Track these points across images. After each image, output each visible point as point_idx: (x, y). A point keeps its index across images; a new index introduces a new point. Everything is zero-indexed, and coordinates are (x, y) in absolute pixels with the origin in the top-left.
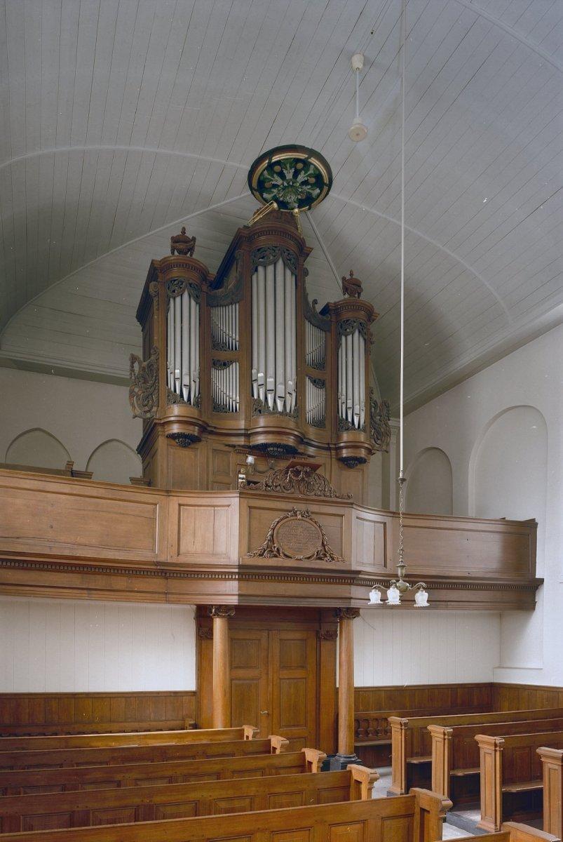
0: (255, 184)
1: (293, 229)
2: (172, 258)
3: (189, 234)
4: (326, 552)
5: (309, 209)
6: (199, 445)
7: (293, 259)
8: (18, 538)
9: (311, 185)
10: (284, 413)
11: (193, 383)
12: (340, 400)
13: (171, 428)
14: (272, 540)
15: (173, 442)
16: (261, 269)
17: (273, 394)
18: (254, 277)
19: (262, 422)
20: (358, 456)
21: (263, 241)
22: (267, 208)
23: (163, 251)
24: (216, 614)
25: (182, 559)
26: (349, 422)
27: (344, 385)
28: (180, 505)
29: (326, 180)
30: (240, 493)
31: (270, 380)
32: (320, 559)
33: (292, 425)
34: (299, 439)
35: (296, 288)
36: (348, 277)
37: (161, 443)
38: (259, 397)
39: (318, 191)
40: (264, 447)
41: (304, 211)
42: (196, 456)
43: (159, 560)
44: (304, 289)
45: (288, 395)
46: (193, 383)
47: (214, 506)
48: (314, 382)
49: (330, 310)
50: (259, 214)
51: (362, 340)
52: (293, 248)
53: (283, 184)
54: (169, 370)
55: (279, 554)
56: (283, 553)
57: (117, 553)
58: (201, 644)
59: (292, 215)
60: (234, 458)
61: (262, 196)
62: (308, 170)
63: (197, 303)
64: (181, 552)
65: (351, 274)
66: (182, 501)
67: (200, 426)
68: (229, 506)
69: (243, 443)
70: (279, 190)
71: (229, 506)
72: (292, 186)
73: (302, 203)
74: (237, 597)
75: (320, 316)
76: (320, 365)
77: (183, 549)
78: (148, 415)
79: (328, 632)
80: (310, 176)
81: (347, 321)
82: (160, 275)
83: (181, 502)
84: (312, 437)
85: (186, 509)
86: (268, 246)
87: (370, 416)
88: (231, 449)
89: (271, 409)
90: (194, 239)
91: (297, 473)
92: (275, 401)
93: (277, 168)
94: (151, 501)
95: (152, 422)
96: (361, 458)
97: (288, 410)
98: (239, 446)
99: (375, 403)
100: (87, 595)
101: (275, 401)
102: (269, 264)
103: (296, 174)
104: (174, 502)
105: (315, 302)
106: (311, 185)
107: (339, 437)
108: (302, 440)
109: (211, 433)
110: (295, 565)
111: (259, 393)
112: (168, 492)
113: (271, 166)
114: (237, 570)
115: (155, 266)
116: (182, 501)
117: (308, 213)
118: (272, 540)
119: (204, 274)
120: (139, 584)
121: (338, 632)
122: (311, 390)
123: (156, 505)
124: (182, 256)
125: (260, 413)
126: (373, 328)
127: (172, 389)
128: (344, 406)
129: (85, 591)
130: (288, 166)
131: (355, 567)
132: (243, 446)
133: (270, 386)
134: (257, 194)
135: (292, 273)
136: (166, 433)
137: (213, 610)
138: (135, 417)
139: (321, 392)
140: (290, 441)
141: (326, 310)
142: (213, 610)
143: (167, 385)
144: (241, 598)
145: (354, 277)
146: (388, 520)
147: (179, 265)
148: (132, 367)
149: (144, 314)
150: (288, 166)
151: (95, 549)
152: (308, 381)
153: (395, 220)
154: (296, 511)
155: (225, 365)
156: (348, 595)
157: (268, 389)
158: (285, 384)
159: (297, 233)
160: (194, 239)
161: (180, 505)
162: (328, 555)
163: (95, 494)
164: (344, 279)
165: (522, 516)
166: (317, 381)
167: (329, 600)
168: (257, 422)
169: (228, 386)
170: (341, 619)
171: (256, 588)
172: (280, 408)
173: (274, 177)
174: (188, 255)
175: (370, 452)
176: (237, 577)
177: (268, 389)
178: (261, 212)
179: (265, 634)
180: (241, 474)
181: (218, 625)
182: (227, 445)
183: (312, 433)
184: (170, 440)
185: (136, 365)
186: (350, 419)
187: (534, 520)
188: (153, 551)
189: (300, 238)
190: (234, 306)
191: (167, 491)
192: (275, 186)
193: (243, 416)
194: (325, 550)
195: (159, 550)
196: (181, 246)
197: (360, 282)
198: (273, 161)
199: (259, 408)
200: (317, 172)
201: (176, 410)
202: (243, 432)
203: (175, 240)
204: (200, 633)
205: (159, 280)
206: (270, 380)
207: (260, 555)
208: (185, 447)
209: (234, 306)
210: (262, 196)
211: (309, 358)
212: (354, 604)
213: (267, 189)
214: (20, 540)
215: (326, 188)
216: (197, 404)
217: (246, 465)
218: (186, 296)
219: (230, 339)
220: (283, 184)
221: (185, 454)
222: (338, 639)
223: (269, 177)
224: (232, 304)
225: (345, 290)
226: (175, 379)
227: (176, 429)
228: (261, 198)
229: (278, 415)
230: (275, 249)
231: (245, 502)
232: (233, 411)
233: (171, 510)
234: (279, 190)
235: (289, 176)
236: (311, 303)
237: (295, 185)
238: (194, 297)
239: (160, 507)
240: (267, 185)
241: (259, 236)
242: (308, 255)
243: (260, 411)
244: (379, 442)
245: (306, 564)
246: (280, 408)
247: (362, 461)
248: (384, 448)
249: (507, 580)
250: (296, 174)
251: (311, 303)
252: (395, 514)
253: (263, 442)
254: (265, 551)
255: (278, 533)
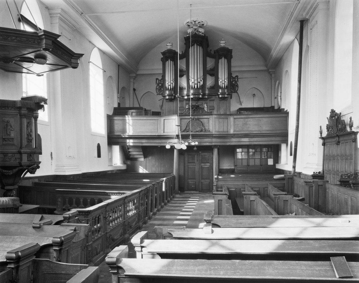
25: (165, 134)
64: (165, 132)
76: (212, 70)
104: (162, 119)
116: (164, 118)
148: (156, 81)
169: (183, 82)
172: (196, 87)
179: (38, 102)
218: (169, 60)
221: (171, 104)
245: (197, 133)
246: (196, 87)
249: (268, 131)
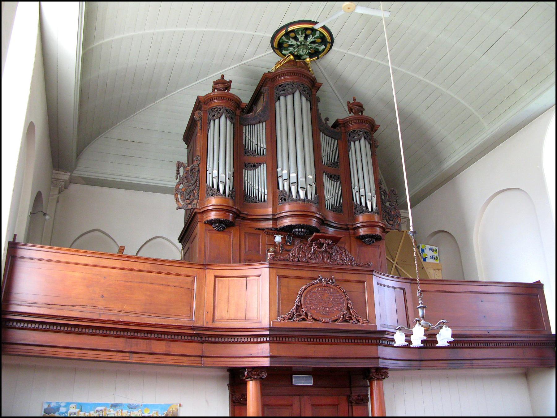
0: (276, 45)
1: (306, 71)
2: (214, 94)
3: (227, 78)
4: (351, 315)
5: (318, 59)
6: (233, 230)
7: (307, 90)
8: (73, 306)
9: (318, 43)
10: (306, 200)
11: (227, 180)
12: (353, 190)
13: (209, 215)
14: (300, 306)
15: (210, 227)
16: (282, 98)
17: (296, 186)
18: (277, 104)
19: (287, 208)
20: (374, 234)
21: (283, 79)
22: (285, 59)
23: (206, 90)
24: (250, 377)
26: (363, 207)
27: (355, 172)
28: (215, 277)
29: (329, 39)
30: (270, 264)
31: (293, 175)
32: (346, 321)
33: (314, 209)
34: (320, 221)
35: (311, 110)
36: (352, 101)
37: (199, 229)
38: (284, 188)
39: (323, 47)
40: (291, 227)
41: (315, 61)
42: (230, 237)
43: (195, 325)
44: (318, 110)
45: (309, 186)
46: (227, 180)
47: (246, 277)
48: (330, 177)
49: (339, 124)
50: (279, 64)
51: (367, 144)
52: (307, 84)
53: (297, 44)
54: (208, 172)
55: (307, 317)
56: (311, 316)
57: (157, 320)
58: (234, 409)
59: (305, 63)
60: (263, 239)
61: (281, 53)
62: (315, 35)
63: (231, 123)
64: (216, 318)
65: (354, 100)
66: (218, 273)
67: (234, 213)
68: (259, 276)
69: (271, 226)
70: (294, 48)
71: (259, 276)
72: (303, 45)
73: (311, 55)
74: (268, 359)
75: (332, 129)
76: (334, 165)
77: (217, 315)
78: (190, 207)
79: (359, 396)
80: (317, 38)
81: (354, 131)
82: (203, 106)
83: (217, 274)
84: (331, 220)
85: (221, 280)
86: (287, 83)
87: (381, 202)
88: (261, 231)
89: (294, 197)
90: (230, 81)
91: (320, 245)
92: (298, 192)
93: (292, 35)
94: (190, 274)
95: (194, 210)
96: (377, 235)
97: (309, 198)
98: (268, 229)
99: (384, 192)
100: (128, 358)
101: (298, 192)
102: (289, 94)
103: (306, 37)
104: (210, 275)
105: (327, 119)
106: (318, 43)
107: (355, 220)
108: (323, 222)
109: (243, 218)
110: (323, 327)
111: (284, 186)
112: (205, 266)
113: (287, 34)
114: (268, 333)
115: (200, 100)
116: (218, 273)
117: (317, 61)
118: (300, 306)
119: (237, 103)
120: (177, 348)
121: (369, 396)
122: (327, 182)
123: (194, 277)
124: (220, 92)
125: (285, 201)
126: (375, 135)
127: (211, 185)
128: (357, 194)
129: (128, 354)
130: (300, 33)
131: (379, 328)
132: (271, 229)
133: (293, 180)
134: (278, 51)
135: (307, 100)
136: (204, 220)
137: (246, 373)
138: (178, 209)
139: (338, 185)
140: (314, 223)
141: (336, 124)
142: (246, 373)
143: (206, 182)
144: (272, 360)
145: (356, 101)
146: (407, 286)
147: (218, 98)
149: (189, 137)
150: (300, 33)
151: (139, 315)
152: (325, 176)
153: (385, 63)
154: (321, 279)
155: (255, 167)
156: (375, 356)
157: (291, 182)
158: (306, 177)
159: (310, 74)
160: (230, 81)
161: (215, 277)
162: (353, 318)
163: (141, 269)
164: (348, 103)
165: (531, 280)
166: (333, 176)
167: (358, 360)
168: (283, 209)
170: (371, 380)
171: (285, 350)
172: (302, 196)
173: (290, 40)
174: (226, 91)
175: (384, 230)
176: (268, 339)
177: (291, 182)
178: (281, 63)
179: (296, 399)
180: (270, 252)
181: (252, 387)
182: (257, 229)
183: (331, 217)
184: (208, 225)
185: (182, 170)
186: (364, 204)
187: (539, 281)
188: (191, 317)
189: (313, 78)
190: (261, 125)
191: (204, 265)
192: (291, 46)
193: (271, 204)
194: (350, 312)
195: (196, 316)
196: (221, 86)
197: (362, 104)
198: (289, 30)
199: (286, 197)
200: (322, 35)
201: (214, 201)
202: (271, 217)
203: (215, 83)
204: (234, 399)
205: (202, 109)
206: (293, 175)
207: (289, 319)
208: (220, 231)
209: (261, 125)
210: (281, 53)
211: (325, 159)
212: (382, 364)
213: (285, 47)
214: (74, 308)
215: (329, 45)
216: (231, 195)
217: (274, 244)
219: (254, 189)
220: (297, 44)
222: (369, 403)
223: (287, 40)
224: (259, 123)
225: (351, 110)
226: (213, 177)
227: (213, 216)
228: (282, 55)
229: (301, 202)
230: (293, 84)
231: (274, 271)
232: (261, 201)
233: (207, 281)
234: (294, 48)
235: (301, 38)
236: (324, 121)
237: (306, 44)
238: (229, 119)
239: (198, 279)
240: (285, 45)
241: (280, 77)
242: (319, 88)
243: (285, 200)
244: (391, 222)
246: (302, 196)
247: (377, 238)
248: (396, 227)
250: (306, 37)
251: (324, 121)
252: (412, 281)
253: (289, 224)
254: (294, 315)
255: (305, 299)
